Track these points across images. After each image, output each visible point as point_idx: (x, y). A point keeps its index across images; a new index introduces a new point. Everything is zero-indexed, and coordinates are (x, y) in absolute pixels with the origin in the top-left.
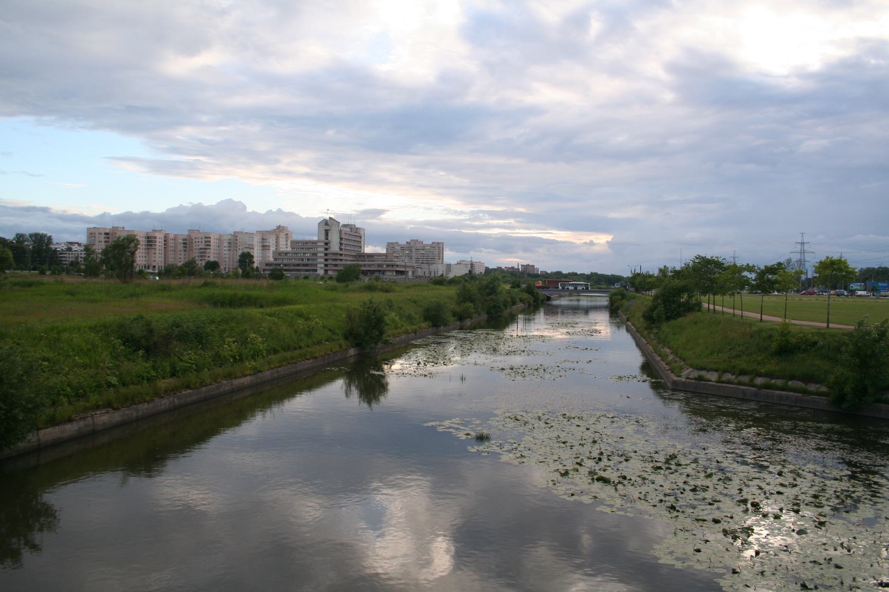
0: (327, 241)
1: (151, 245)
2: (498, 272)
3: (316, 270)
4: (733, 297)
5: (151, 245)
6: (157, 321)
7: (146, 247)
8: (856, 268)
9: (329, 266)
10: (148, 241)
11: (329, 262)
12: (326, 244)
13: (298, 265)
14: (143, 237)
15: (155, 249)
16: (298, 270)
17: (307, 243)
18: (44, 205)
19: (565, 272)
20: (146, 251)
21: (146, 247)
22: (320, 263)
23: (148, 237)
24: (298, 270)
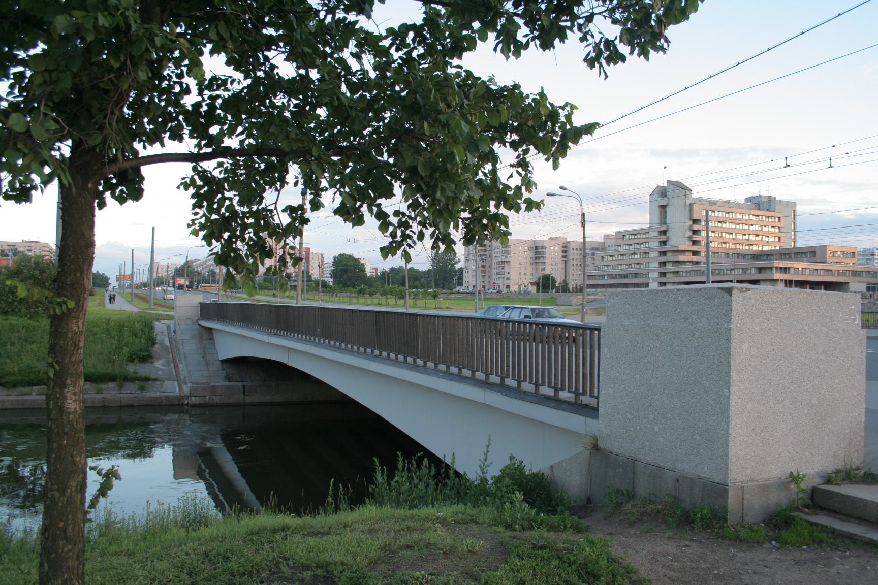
0: (664, 228)
1: (539, 258)
2: (66, 218)
3: (647, 285)
4: (298, 237)
5: (539, 258)
6: (575, 501)
7: (533, 261)
8: (668, 45)
9: (667, 275)
10: (536, 253)
11: (669, 267)
12: (664, 232)
13: (625, 276)
14: (577, 249)
15: (544, 263)
16: (626, 286)
17: (635, 233)
18: (9, 201)
19: (13, 201)
20: (534, 266)
21: (532, 261)
22: (654, 270)
23: (536, 248)
24: (626, 286)
